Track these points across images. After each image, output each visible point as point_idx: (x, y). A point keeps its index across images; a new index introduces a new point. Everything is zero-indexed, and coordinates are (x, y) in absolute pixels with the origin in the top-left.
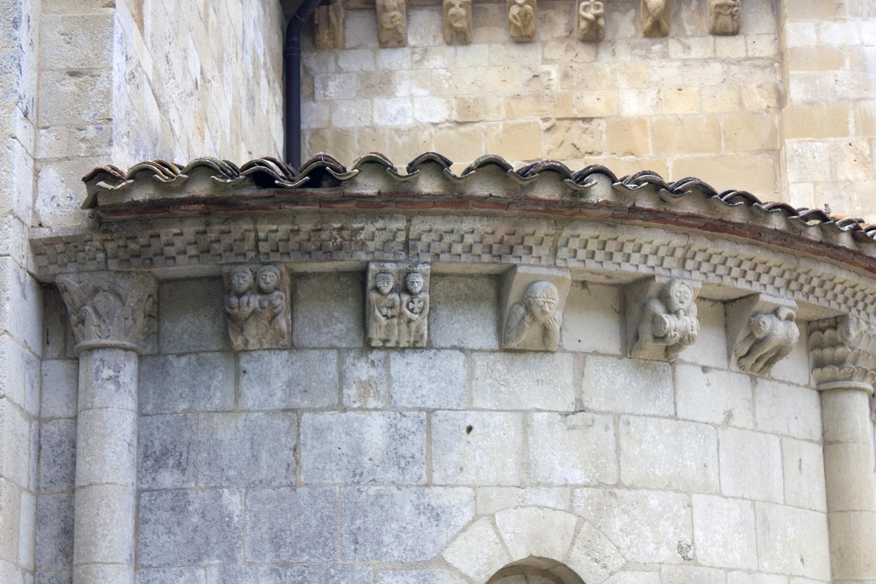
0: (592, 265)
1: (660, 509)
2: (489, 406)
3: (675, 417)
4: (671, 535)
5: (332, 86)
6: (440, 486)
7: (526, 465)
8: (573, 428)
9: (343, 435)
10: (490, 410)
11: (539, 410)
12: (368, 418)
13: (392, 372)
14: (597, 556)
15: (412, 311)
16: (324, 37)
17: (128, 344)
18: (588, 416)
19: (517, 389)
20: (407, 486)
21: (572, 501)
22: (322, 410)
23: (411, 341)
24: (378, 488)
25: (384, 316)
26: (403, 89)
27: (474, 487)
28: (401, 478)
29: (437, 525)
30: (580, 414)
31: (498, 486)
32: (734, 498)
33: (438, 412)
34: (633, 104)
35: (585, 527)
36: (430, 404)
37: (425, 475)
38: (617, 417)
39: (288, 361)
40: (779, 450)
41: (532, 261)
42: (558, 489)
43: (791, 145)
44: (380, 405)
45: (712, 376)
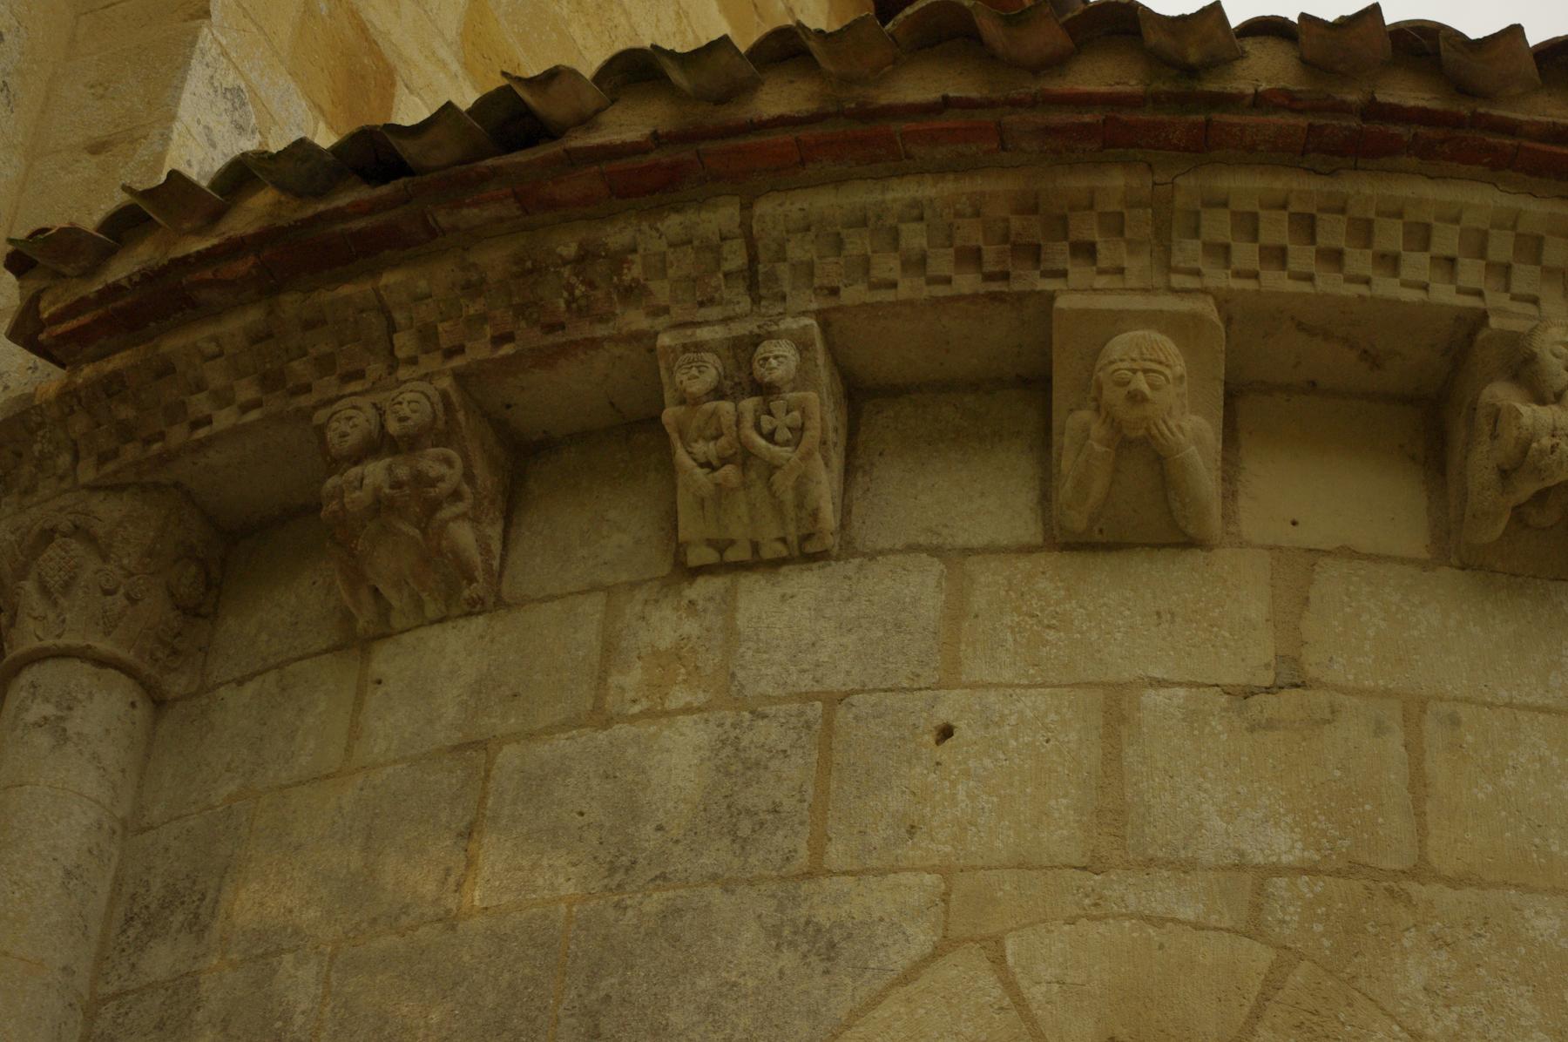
0: (1276, 281)
2: (1008, 675)
6: (844, 873)
8: (1270, 725)
9: (594, 782)
10: (1010, 686)
11: (1160, 683)
12: (666, 733)
13: (741, 622)
15: (770, 437)
17: (104, 646)
18: (1319, 698)
19: (1094, 636)
20: (751, 883)
21: (1258, 908)
22: (550, 731)
23: (793, 538)
24: (671, 894)
25: (702, 465)
27: (945, 871)
28: (737, 863)
29: (826, 972)
31: (1020, 866)
33: (855, 699)
35: (1300, 975)
36: (835, 682)
37: (804, 851)
38: (1414, 709)
39: (482, 637)
41: (1101, 281)
42: (1211, 875)
44: (701, 698)
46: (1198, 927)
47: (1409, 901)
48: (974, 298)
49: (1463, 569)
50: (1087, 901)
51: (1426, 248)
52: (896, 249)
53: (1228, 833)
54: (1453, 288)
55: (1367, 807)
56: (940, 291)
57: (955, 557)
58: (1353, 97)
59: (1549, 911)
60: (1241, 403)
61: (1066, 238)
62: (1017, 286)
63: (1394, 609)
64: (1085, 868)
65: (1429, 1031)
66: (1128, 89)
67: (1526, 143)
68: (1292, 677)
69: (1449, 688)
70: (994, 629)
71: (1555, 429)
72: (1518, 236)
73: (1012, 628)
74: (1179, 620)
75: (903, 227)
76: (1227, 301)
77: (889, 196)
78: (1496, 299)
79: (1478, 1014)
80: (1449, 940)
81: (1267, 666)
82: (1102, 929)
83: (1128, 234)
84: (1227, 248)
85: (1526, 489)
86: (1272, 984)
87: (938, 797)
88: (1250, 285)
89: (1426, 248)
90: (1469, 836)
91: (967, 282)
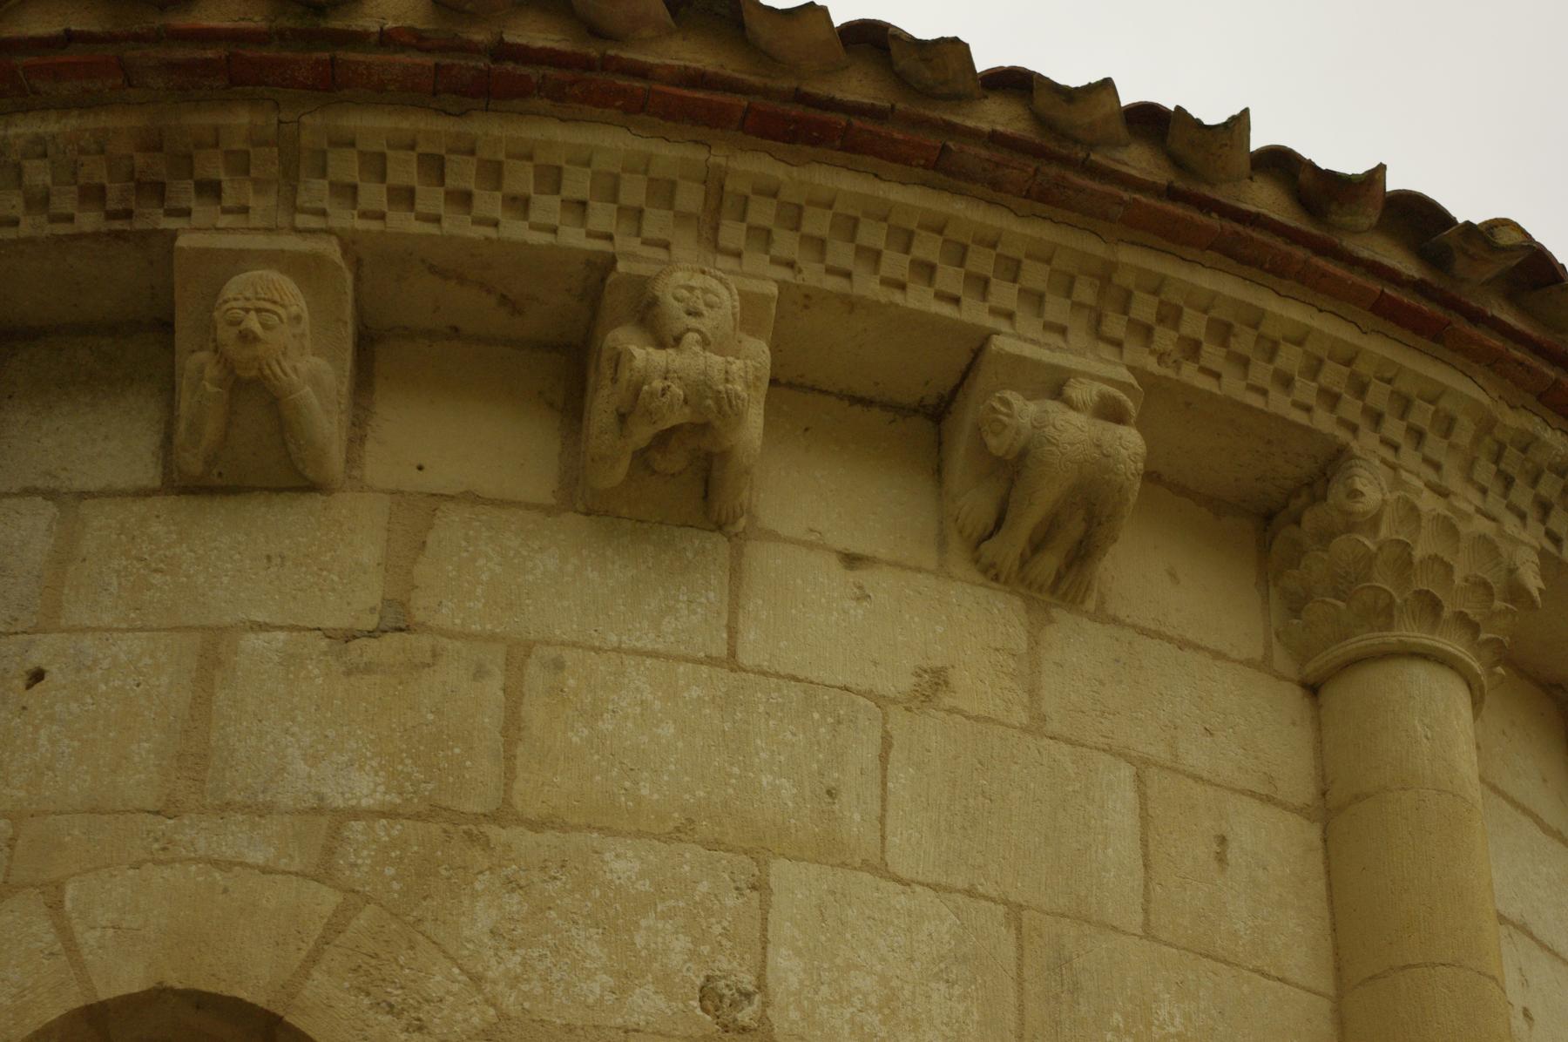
0: (403, 223)
1: (645, 886)
2: (107, 619)
3: (731, 661)
4: (676, 960)
8: (368, 669)
14: (396, 996)
18: (424, 642)
21: (330, 851)
30: (394, 639)
31: (92, 811)
32: (935, 887)
38: (518, 653)
40: (1131, 795)
41: (225, 220)
42: (287, 819)
45: (879, 582)
46: (265, 870)
47: (487, 845)
48: (96, 236)
49: (587, 514)
50: (156, 846)
51: (558, 192)
52: (20, 186)
53: (309, 776)
54: (583, 231)
55: (457, 751)
56: (62, 229)
57: (68, 499)
58: (480, 36)
59: (630, 854)
60: (372, 350)
61: (191, 175)
62: (139, 225)
63: (512, 553)
64: (158, 813)
65: (490, 974)
66: (252, 25)
67: (657, 87)
68: (398, 620)
69: (558, 632)
70: (101, 573)
71: (668, 371)
72: (651, 180)
73: (118, 572)
74: (289, 564)
75: (26, 163)
76: (354, 242)
77: (12, 131)
78: (626, 243)
79: (542, 957)
80: (523, 883)
81: (372, 610)
82: (167, 872)
83: (253, 173)
84: (354, 188)
85: (642, 434)
86: (334, 927)
87: (18, 742)
88: (375, 226)
89: (558, 192)
90: (557, 780)
91: (89, 221)
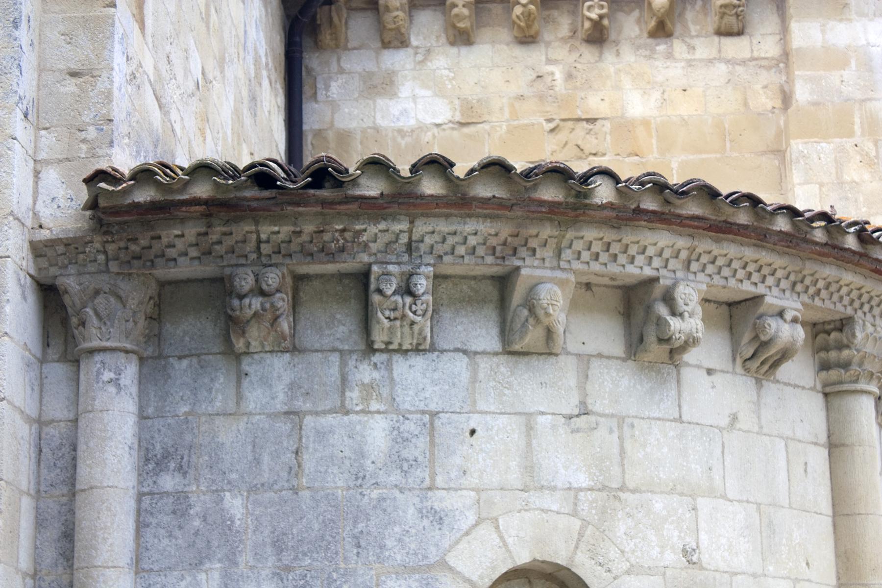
0: (596, 267)
1: (664, 513)
2: (493, 408)
3: (680, 420)
4: (675, 539)
5: (334, 87)
6: (443, 489)
7: (530, 468)
8: (577, 431)
9: (345, 438)
10: (494, 413)
11: (543, 413)
12: (371, 421)
13: (395, 375)
14: (601, 560)
15: (415, 313)
16: (326, 37)
17: (129, 346)
18: (592, 418)
19: (521, 392)
20: (410, 490)
21: (575, 504)
22: (325, 412)
23: (414, 344)
24: (380, 491)
25: (386, 318)
26: (406, 89)
27: (477, 490)
28: (404, 481)
29: (440, 529)
30: (584, 417)
31: (501, 489)
32: (739, 501)
33: (441, 415)
34: (638, 105)
35: (589, 530)
36: (433, 407)
37: (428, 478)
38: (621, 420)
39: (289, 363)
40: (784, 453)
41: (536, 263)
42: (561, 492)
43: (797, 146)
44: (382, 408)
45: (717, 378)
